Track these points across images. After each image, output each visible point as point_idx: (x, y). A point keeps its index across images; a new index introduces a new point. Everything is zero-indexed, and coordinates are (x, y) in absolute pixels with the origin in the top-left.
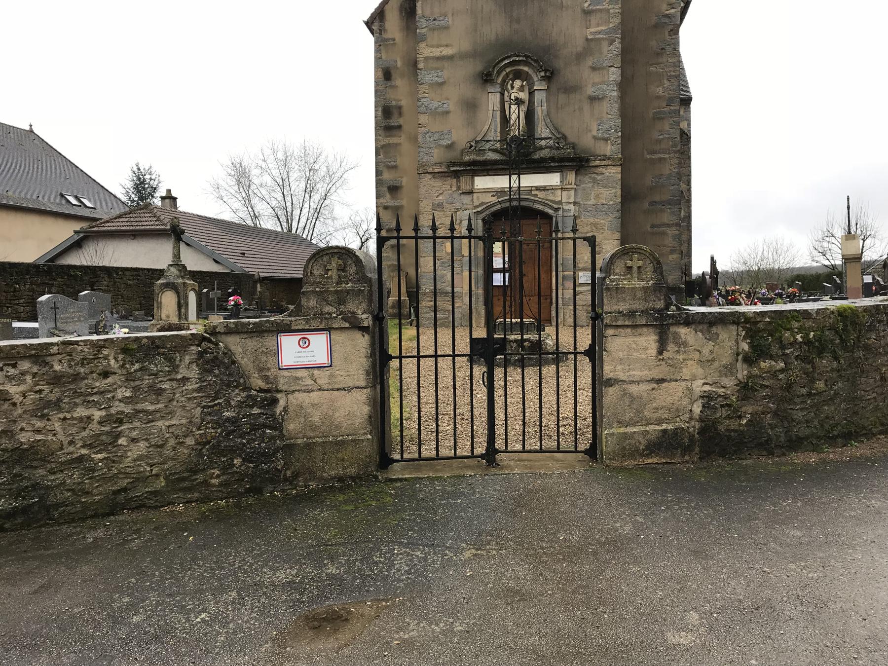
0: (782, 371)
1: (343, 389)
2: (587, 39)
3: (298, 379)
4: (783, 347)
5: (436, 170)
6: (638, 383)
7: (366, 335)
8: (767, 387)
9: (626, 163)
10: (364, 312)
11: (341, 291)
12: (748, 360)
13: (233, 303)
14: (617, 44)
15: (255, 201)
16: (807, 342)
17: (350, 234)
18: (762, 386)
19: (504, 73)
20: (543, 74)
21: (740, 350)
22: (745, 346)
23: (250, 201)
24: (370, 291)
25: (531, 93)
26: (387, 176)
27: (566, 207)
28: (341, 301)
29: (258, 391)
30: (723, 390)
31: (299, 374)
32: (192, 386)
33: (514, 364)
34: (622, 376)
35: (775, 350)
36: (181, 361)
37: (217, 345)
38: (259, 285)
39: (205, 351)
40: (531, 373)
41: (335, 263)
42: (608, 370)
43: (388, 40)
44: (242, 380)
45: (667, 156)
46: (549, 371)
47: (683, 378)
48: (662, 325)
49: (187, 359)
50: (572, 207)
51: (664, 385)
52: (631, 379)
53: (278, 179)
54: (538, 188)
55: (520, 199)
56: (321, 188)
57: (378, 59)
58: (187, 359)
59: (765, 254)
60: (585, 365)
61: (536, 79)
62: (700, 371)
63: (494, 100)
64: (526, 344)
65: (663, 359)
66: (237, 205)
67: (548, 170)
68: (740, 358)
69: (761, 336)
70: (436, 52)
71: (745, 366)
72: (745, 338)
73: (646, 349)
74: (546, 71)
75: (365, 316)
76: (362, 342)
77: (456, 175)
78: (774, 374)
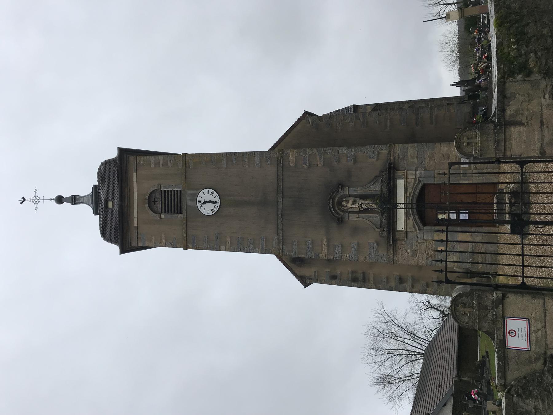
0: (536, 54)
1: (545, 313)
2: (323, 165)
3: (537, 340)
4: (521, 55)
5: (392, 253)
6: (543, 136)
7: (508, 295)
8: (546, 62)
9: (392, 141)
10: (492, 295)
11: (479, 307)
12: (529, 74)
13: (476, 396)
14: (327, 149)
15: (401, 374)
16: (517, 42)
17: (426, 314)
18: (546, 64)
19: (338, 211)
20: (340, 190)
21: (522, 79)
22: (519, 77)
23: (401, 378)
24: (479, 290)
25: (350, 196)
26: (393, 284)
27: (418, 175)
28: (485, 308)
29: (545, 366)
30: (548, 87)
31: (534, 338)
32: (540, 405)
33: (528, 209)
34: (538, 146)
35: (522, 60)
36: (523, 408)
37: (512, 386)
38: (463, 379)
39: (517, 393)
40: (534, 198)
41: (460, 308)
42: (534, 153)
43: (315, 275)
44: (538, 374)
45: (389, 118)
46: (533, 188)
47: (540, 110)
48: (504, 124)
49: (521, 404)
50: (418, 172)
51: (544, 121)
52: (540, 140)
53: (388, 357)
54: (406, 192)
55: (412, 203)
56: (395, 329)
57: (325, 282)
58: (521, 404)
59: (449, 50)
60: (528, 167)
61: (342, 193)
62: (535, 101)
63: (353, 217)
64: (513, 201)
65: (527, 123)
66: (403, 387)
67: (395, 186)
68: (527, 79)
69: (512, 68)
70: (325, 248)
71: (533, 75)
72: (514, 77)
73: (520, 132)
74: (338, 188)
75: (495, 295)
76: (512, 298)
77: (395, 241)
78: (538, 58)
